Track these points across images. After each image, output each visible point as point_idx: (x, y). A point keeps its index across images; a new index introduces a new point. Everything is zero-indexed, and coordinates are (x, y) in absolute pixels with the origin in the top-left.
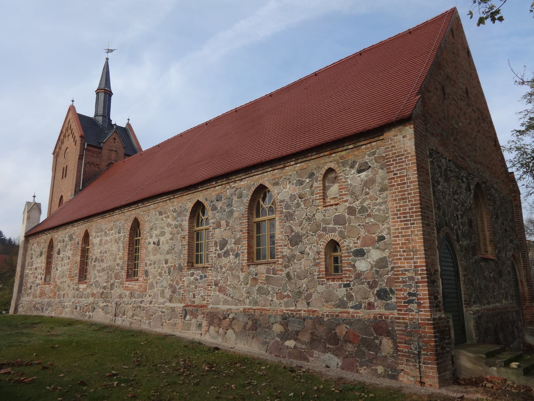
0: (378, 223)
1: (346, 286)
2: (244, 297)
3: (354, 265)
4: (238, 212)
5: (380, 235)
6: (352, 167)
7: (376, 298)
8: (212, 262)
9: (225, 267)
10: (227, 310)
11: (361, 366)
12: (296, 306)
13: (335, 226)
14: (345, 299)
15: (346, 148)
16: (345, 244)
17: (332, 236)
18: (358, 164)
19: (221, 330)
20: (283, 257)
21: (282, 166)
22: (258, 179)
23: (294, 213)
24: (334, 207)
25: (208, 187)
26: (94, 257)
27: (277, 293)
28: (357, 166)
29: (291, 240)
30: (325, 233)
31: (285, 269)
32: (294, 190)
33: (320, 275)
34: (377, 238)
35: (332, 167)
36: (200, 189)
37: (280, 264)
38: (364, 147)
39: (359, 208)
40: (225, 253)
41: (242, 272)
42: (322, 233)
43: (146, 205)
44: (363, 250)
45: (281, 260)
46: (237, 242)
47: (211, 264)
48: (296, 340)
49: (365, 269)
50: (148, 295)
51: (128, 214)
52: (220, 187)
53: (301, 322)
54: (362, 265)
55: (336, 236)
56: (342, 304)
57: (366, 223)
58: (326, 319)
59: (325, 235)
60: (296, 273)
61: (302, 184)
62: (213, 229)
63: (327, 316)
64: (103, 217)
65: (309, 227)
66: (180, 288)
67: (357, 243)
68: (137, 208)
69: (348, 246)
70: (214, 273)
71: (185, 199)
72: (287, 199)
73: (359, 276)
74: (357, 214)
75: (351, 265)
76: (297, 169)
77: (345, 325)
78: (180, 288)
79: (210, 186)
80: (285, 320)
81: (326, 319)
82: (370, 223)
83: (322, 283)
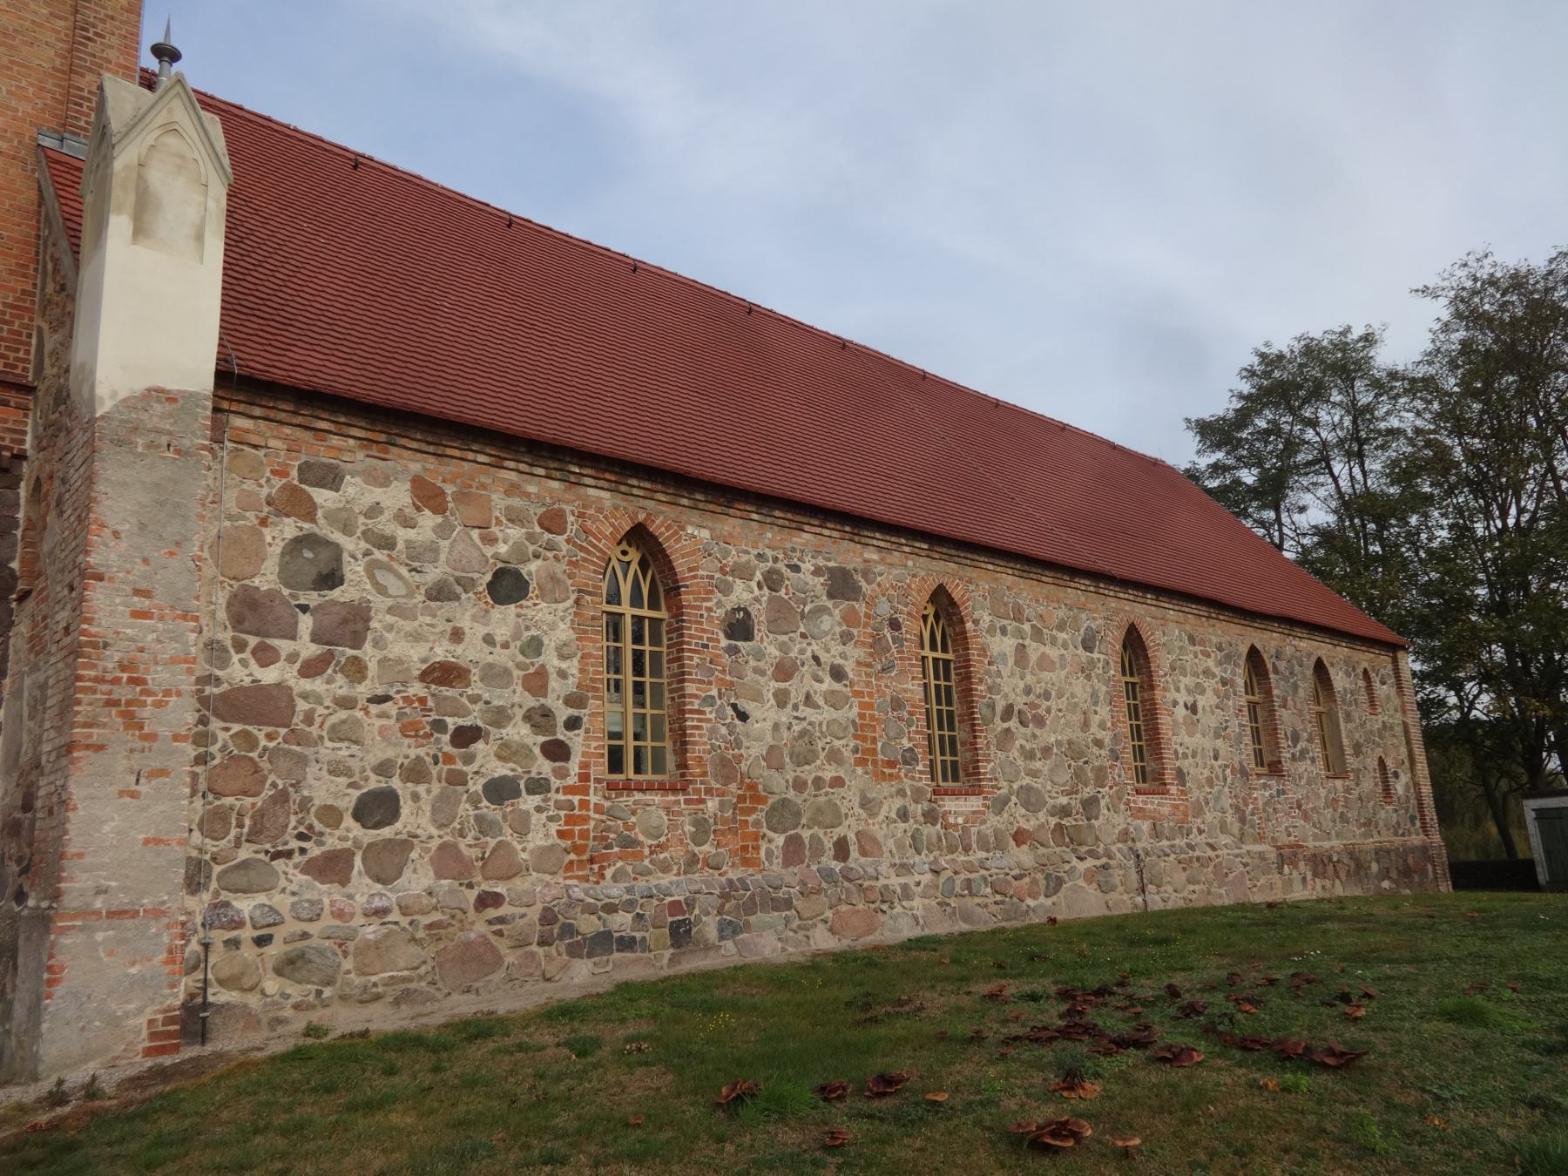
22: (1318, 648)
26: (1000, 705)
43: (1163, 604)
50: (1195, 830)
51: (1113, 605)
64: (1025, 575)
66: (1253, 814)
68: (1139, 599)
78: (1253, 814)
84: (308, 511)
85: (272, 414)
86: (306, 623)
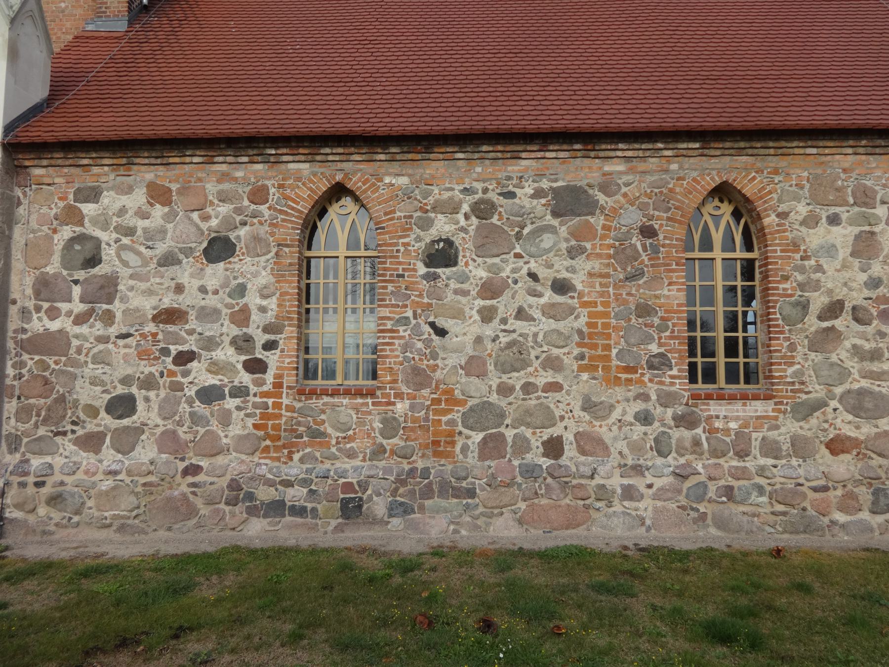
43: (171, 160)
84: (78, 219)
85: (53, 162)
86: (77, 291)
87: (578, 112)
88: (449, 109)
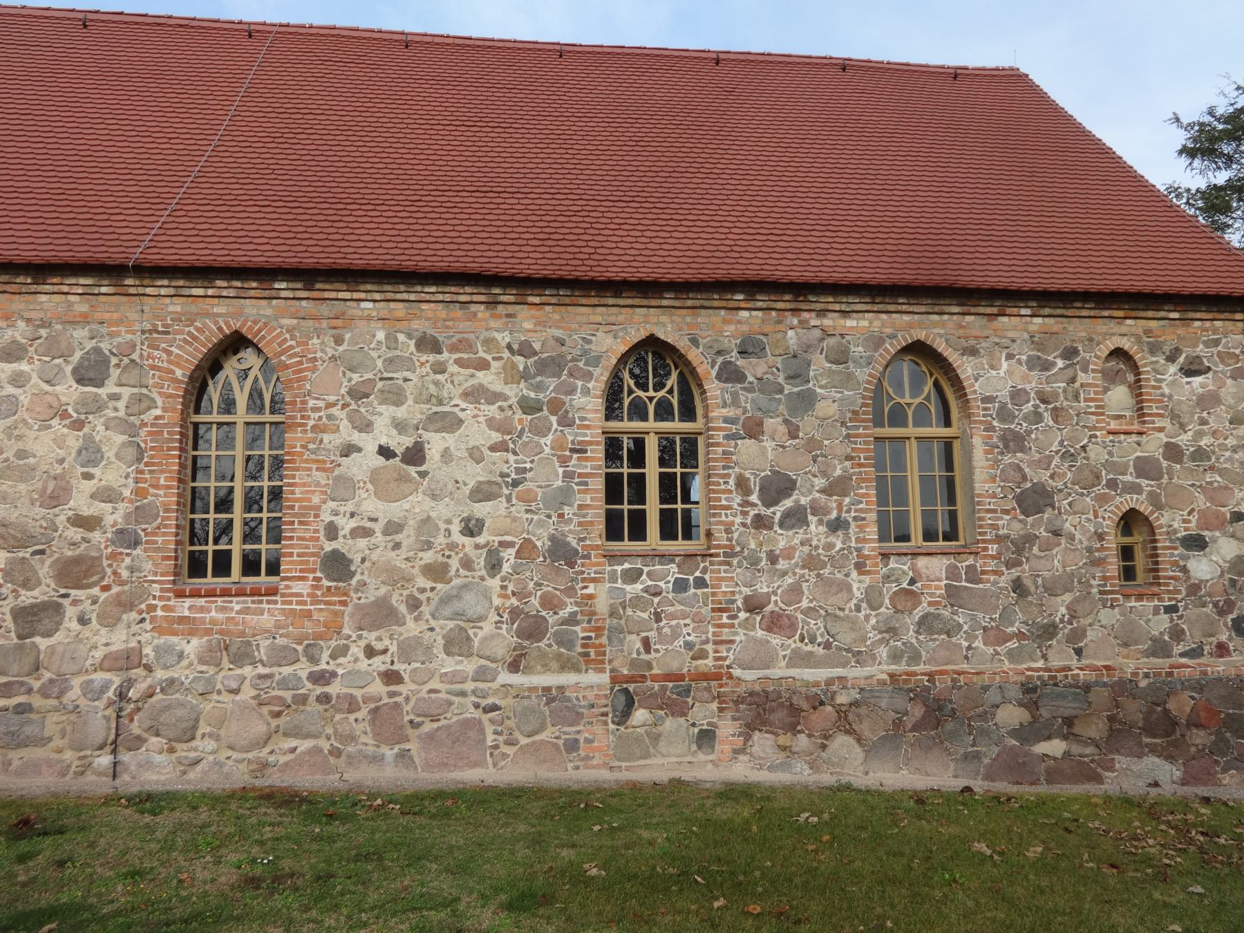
0: (1231, 486)
1: (1171, 610)
2: (869, 643)
3: (1185, 566)
4: (834, 401)
5: (1236, 509)
6: (1171, 359)
7: (1233, 634)
8: (730, 540)
9: (790, 557)
10: (829, 682)
11: (1225, 770)
12: (1046, 660)
13: (1138, 481)
14: (1166, 638)
15: (1162, 314)
16: (1162, 521)
17: (1132, 500)
18: (1184, 356)
19: (802, 741)
20: (999, 539)
21: (995, 310)
22: (911, 326)
23: (1029, 435)
24: (1134, 438)
25: (706, 303)
27: (985, 629)
28: (1182, 359)
29: (1020, 500)
30: (1113, 493)
31: (1008, 569)
32: (1025, 378)
33: (1105, 585)
34: (1228, 515)
35: (1126, 348)
36: (665, 303)
37: (993, 557)
38: (1197, 324)
39: (1192, 449)
40: (787, 515)
41: (861, 573)
42: (1107, 491)
43: (327, 295)
44: (1203, 537)
45: (995, 546)
46: (838, 487)
47: (725, 546)
48: (1065, 738)
49: (1208, 577)
52: (760, 314)
53: (1078, 694)
54: (1202, 568)
55: (1142, 502)
56: (1159, 648)
57: (1207, 483)
58: (1143, 683)
59: (1113, 498)
60: (1040, 580)
61: (1047, 369)
62: (727, 437)
63: (1147, 675)
65: (1069, 475)
67: (1189, 522)
69: (1170, 526)
70: (738, 573)
71: (584, 319)
72: (1004, 394)
73: (1194, 589)
74: (1185, 460)
75: (1178, 566)
76: (1032, 328)
77: (1188, 693)
79: (716, 304)
80: (1031, 693)
81: (1143, 683)
82: (1216, 485)
83: (1112, 605)
87: (658, 185)
88: (417, 157)
